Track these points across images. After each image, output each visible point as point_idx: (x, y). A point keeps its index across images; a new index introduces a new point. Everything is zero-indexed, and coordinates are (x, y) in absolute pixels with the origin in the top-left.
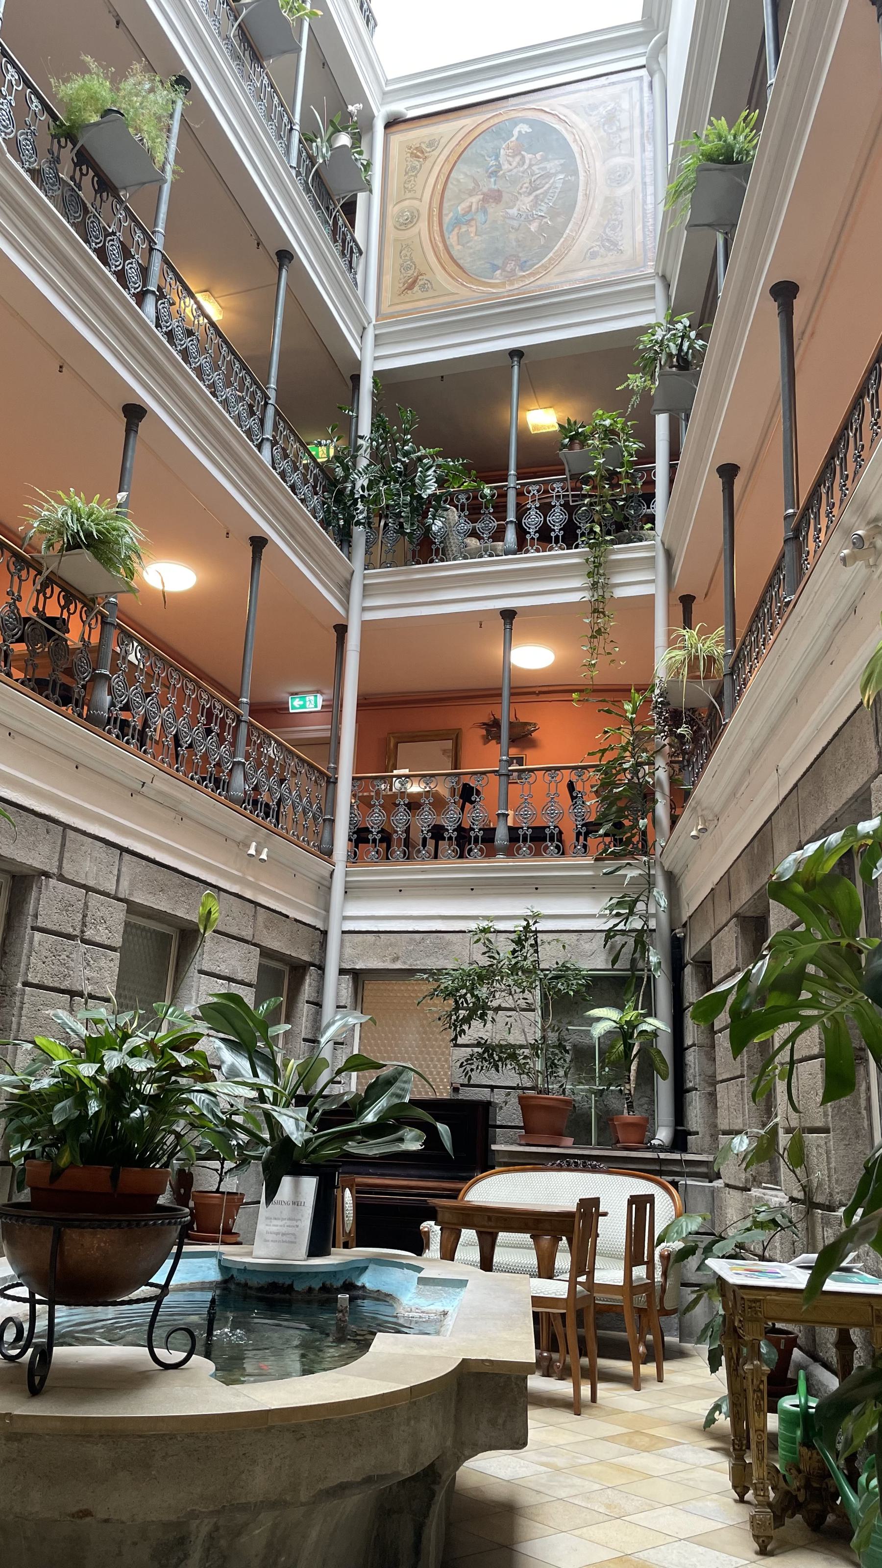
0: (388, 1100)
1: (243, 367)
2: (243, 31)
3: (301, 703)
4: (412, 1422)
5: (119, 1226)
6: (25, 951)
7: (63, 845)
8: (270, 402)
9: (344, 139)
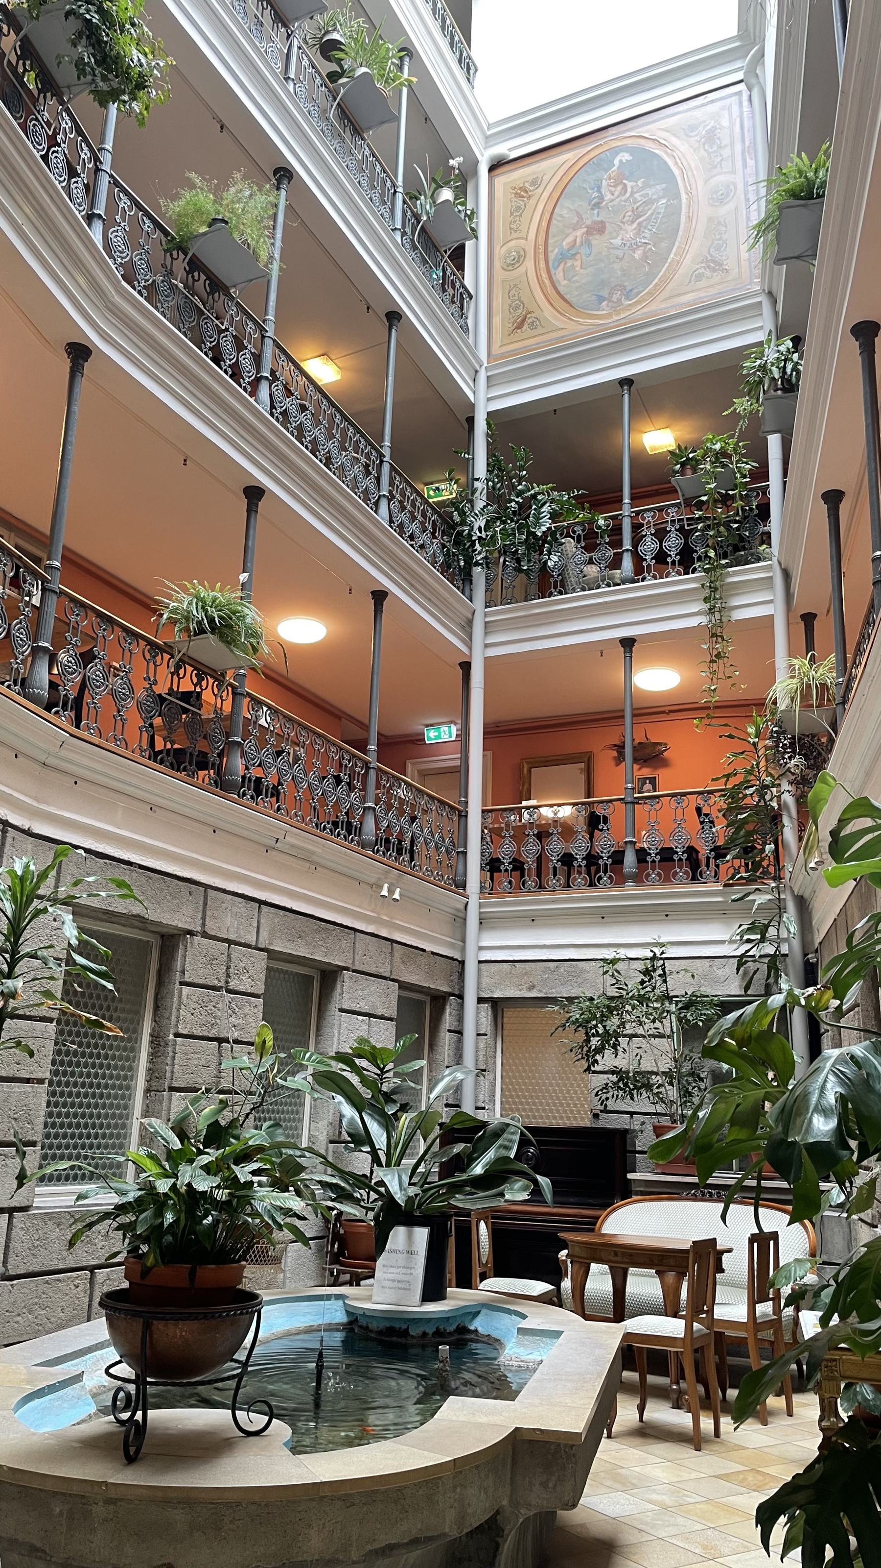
0: (496, 1152)
1: (358, 431)
2: (343, 111)
3: (436, 734)
4: (458, 1490)
5: (196, 1319)
7: (205, 904)
8: (385, 459)
9: (446, 194)
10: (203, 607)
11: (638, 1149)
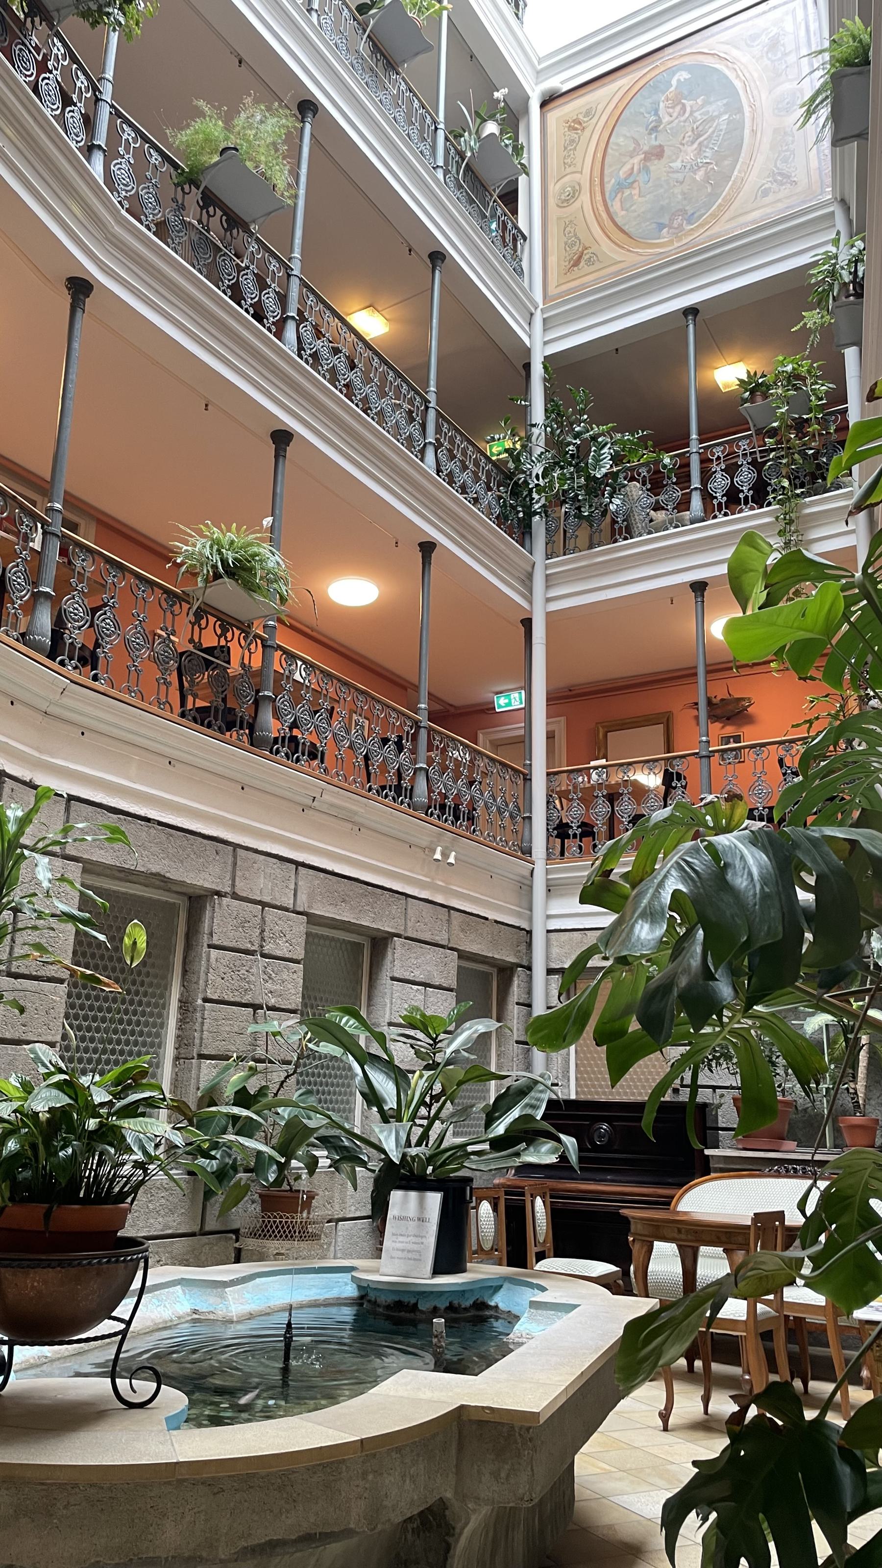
1: (398, 375)
2: (375, 45)
3: (507, 701)
4: (370, 1477)
6: (203, 968)
7: (235, 864)
8: (431, 405)
9: (491, 128)
10: (219, 551)
11: (721, 1125)
